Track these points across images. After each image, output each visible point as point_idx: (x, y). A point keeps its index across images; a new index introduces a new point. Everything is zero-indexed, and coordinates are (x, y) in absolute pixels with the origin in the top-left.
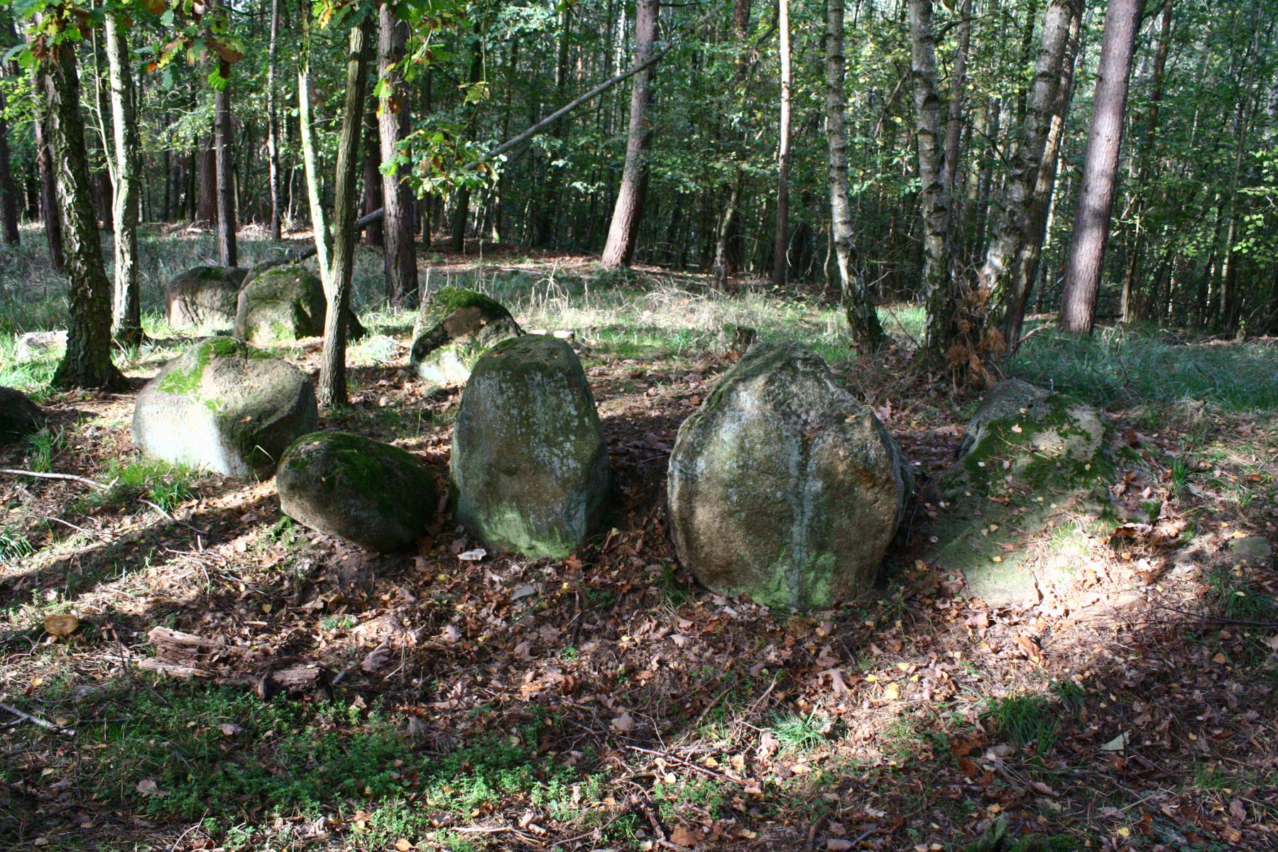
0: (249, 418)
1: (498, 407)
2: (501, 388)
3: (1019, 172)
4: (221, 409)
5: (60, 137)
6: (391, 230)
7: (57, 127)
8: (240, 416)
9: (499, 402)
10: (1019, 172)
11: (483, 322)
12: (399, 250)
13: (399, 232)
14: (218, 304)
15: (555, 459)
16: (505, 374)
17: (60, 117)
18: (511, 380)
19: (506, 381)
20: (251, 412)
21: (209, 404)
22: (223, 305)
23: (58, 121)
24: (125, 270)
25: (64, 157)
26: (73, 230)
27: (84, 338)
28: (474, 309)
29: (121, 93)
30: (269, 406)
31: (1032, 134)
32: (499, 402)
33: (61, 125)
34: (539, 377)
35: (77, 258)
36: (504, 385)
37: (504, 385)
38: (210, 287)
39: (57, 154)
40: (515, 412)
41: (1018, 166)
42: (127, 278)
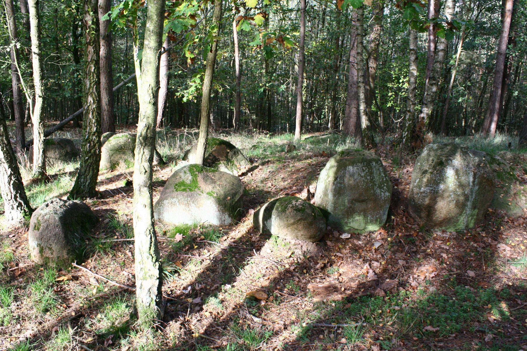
0: (229, 198)
1: (362, 177)
2: (363, 169)
3: (434, 82)
4: (215, 195)
5: (93, 76)
6: (105, 117)
7: (93, 71)
8: (225, 197)
9: (363, 174)
10: (434, 82)
11: (229, 151)
12: (109, 126)
13: (109, 118)
14: (58, 156)
15: (382, 193)
16: (364, 164)
17: (95, 66)
18: (366, 166)
19: (365, 167)
20: (228, 195)
21: (209, 194)
22: (60, 157)
23: (93, 68)
24: (41, 142)
25: (94, 85)
26: (94, 120)
27: (91, 174)
28: (223, 146)
29: (38, 55)
30: (234, 191)
31: (439, 69)
32: (363, 174)
33: (94, 70)
34: (374, 164)
35: (94, 135)
36: (364, 168)
37: (364, 168)
38: (52, 149)
39: (90, 84)
40: (369, 178)
41: (434, 80)
42: (42, 146)
